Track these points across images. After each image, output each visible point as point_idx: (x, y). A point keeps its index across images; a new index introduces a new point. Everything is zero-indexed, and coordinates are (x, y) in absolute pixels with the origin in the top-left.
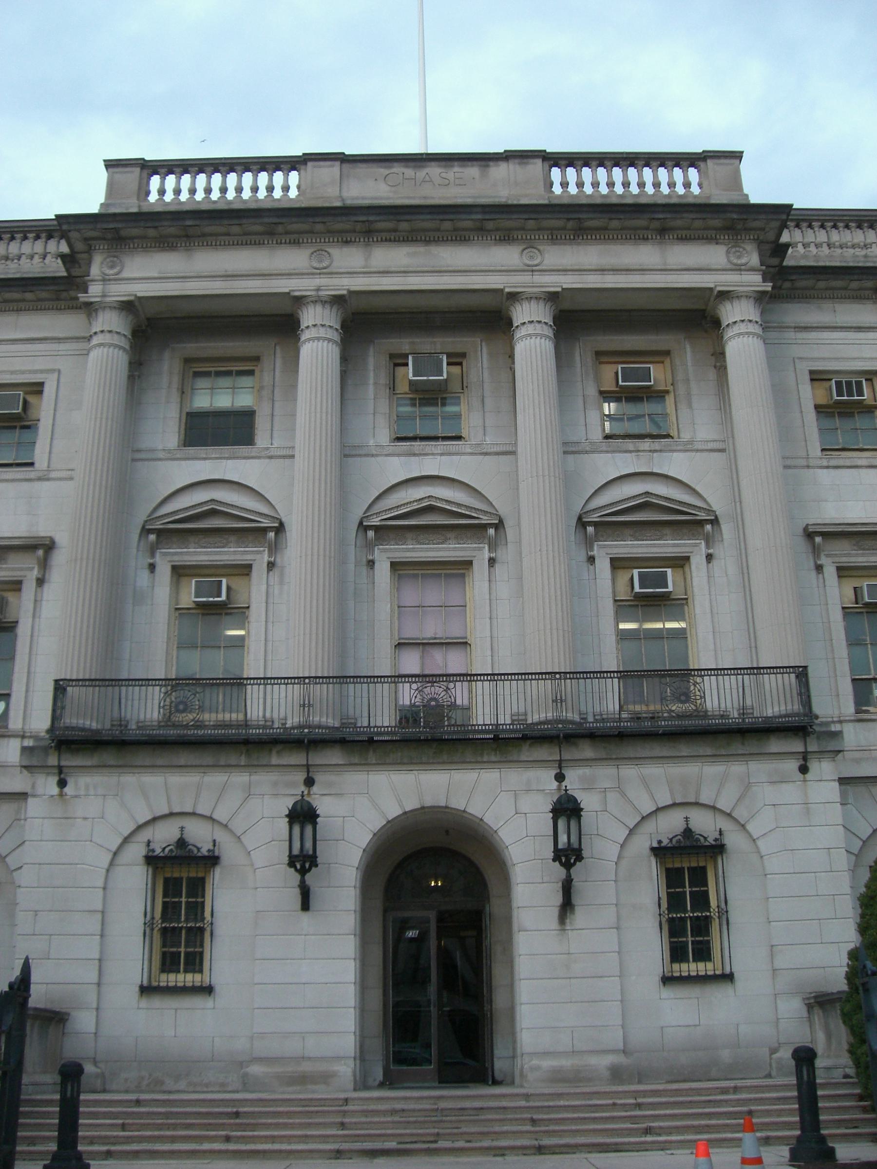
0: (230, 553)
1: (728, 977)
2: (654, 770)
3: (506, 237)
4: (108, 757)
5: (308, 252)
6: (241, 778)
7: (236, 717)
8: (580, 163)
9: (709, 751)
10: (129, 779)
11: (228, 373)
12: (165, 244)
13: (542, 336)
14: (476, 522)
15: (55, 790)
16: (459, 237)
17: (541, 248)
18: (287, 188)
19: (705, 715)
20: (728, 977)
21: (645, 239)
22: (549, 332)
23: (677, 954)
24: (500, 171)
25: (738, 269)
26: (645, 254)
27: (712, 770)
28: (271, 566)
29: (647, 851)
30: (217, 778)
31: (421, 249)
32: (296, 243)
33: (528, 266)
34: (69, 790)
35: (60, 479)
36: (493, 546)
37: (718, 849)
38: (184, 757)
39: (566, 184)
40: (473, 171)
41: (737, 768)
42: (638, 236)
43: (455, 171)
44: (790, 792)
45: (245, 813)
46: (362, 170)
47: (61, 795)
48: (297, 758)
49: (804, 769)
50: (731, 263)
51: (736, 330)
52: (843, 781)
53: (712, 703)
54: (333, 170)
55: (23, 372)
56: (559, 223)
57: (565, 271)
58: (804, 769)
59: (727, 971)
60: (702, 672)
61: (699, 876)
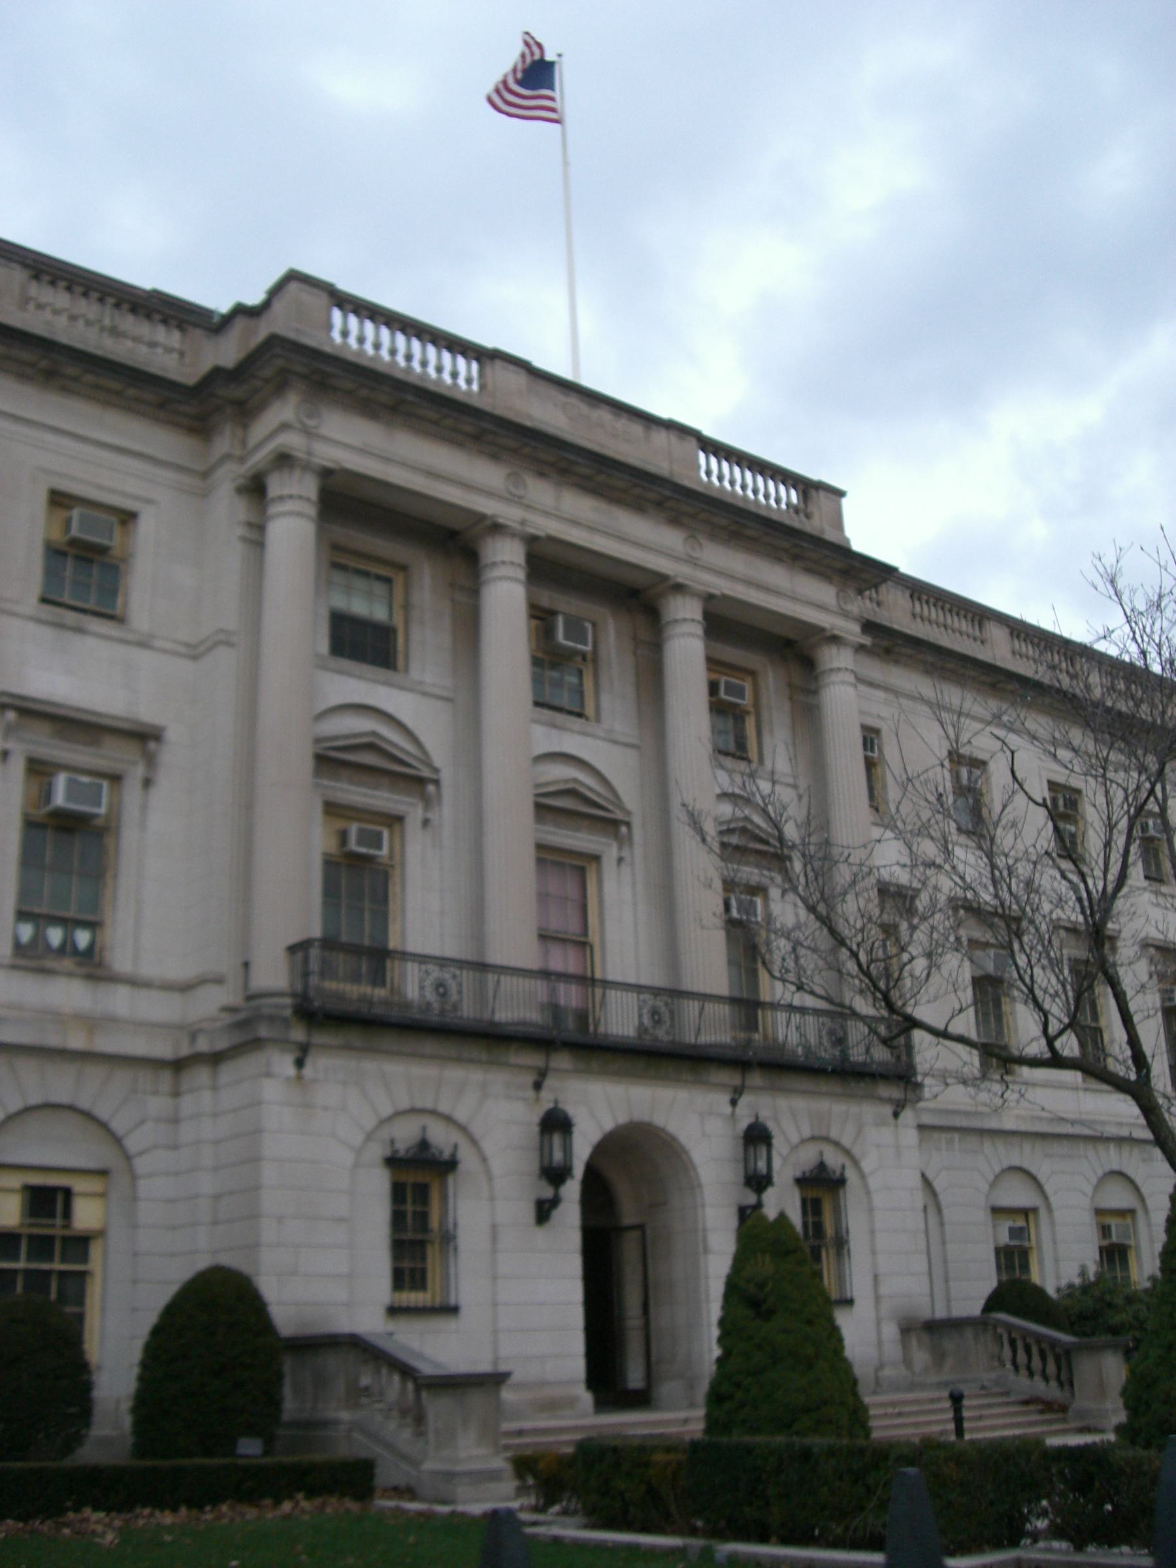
0: (383, 799)
1: (452, 1310)
2: (800, 1104)
3: (675, 520)
4: (355, 1037)
5: (508, 471)
6: (476, 1075)
7: (380, 993)
8: (770, 473)
9: (484, 1056)
10: (370, 1065)
11: (366, 574)
12: (369, 408)
13: (299, 514)
14: (601, 813)
15: (291, 1071)
16: (638, 506)
17: (702, 541)
18: (459, 376)
19: (407, 1005)
20: (452, 1310)
21: (780, 560)
22: (312, 511)
23: (400, 1279)
24: (660, 438)
25: (845, 615)
26: (776, 575)
27: (839, 1108)
28: (426, 822)
29: (791, 1182)
30: (455, 1073)
31: (603, 506)
32: (495, 457)
33: (511, 494)
34: (308, 1071)
35: (165, 651)
36: (427, 802)
37: (450, 1165)
38: (429, 1046)
39: (712, 473)
40: (637, 429)
41: (854, 1108)
42: (776, 555)
43: (623, 424)
44: (885, 1135)
45: (490, 1116)
46: (542, 387)
47: (299, 1077)
48: (534, 1059)
49: (896, 1115)
50: (840, 607)
51: (289, 506)
52: (921, 1128)
53: (412, 992)
54: (519, 380)
55: (113, 491)
56: (724, 522)
57: (732, 578)
58: (896, 1115)
59: (452, 1302)
60: (404, 956)
61: (422, 1193)
